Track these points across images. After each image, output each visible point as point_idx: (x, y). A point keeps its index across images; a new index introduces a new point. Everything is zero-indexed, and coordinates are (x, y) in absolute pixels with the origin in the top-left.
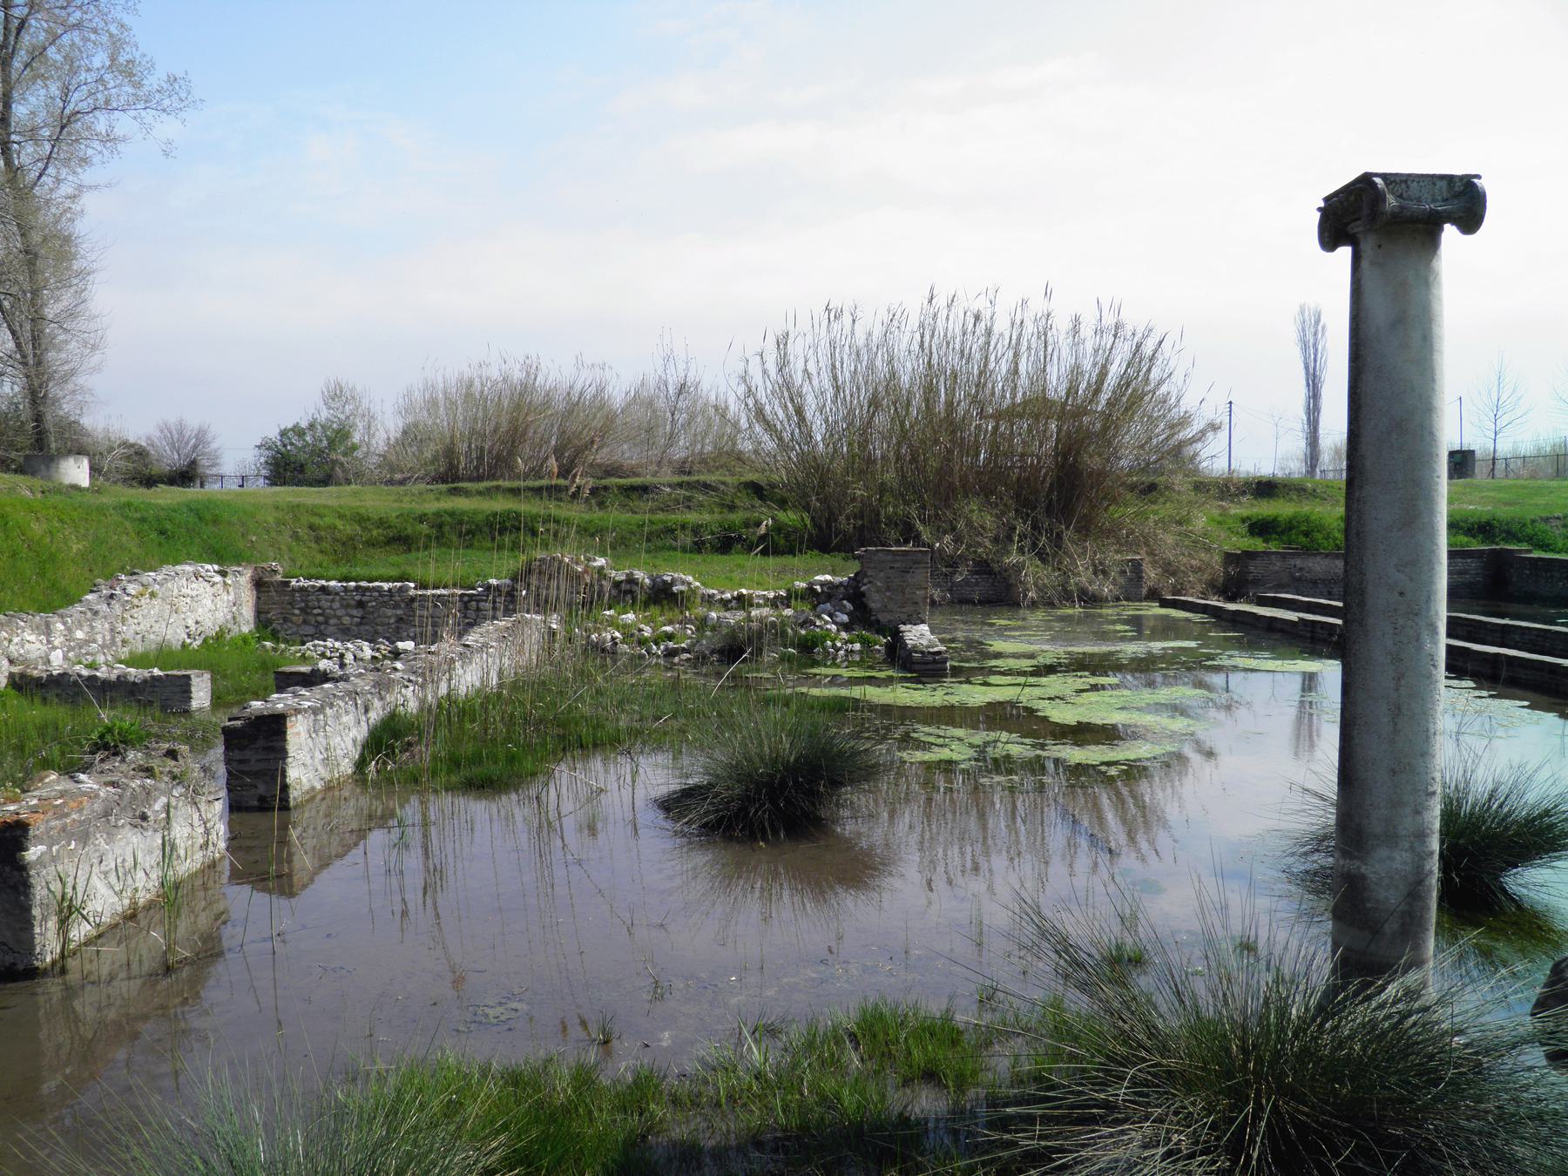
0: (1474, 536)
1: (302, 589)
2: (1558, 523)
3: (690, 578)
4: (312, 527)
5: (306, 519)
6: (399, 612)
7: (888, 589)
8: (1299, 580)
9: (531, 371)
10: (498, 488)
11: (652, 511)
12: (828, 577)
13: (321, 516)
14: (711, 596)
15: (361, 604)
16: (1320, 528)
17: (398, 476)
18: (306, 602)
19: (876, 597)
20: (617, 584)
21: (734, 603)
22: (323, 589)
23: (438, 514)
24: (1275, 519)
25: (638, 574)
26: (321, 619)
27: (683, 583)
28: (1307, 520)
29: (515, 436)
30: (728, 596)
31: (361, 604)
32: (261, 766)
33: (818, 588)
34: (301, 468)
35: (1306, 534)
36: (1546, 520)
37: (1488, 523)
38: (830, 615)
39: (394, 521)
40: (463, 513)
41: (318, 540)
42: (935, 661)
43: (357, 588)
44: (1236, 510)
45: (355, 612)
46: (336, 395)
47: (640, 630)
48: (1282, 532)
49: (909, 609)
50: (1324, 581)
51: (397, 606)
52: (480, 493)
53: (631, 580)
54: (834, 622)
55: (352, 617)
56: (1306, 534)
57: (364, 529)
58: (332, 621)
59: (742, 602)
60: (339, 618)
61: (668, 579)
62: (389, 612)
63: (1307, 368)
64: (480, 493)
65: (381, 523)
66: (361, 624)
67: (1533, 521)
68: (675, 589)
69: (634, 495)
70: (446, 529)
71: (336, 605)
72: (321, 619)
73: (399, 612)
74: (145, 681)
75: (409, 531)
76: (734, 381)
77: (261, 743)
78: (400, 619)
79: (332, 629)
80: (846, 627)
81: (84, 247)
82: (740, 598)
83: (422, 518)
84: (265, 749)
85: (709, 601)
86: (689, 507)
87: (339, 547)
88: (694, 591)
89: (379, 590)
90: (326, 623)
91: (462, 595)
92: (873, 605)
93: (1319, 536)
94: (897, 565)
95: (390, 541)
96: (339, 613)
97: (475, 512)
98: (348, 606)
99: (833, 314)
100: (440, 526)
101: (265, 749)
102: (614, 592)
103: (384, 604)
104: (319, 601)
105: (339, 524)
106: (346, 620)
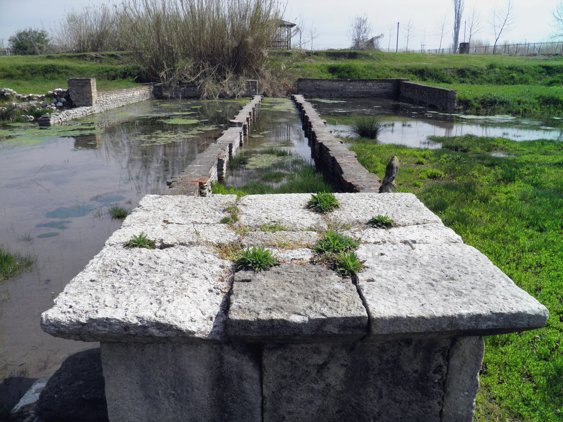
0: (416, 75)
2: (450, 70)
3: (11, 90)
7: (77, 93)
12: (60, 89)
14: (19, 97)
19: (73, 96)
27: (8, 92)
30: (26, 96)
33: (56, 93)
34: (26, 49)
35: (348, 72)
36: (446, 69)
37: (423, 70)
42: (45, 120)
44: (319, 63)
46: (360, 26)
48: (339, 72)
49: (86, 101)
50: (328, 90)
52: (58, 58)
54: (56, 106)
56: (348, 72)
59: (30, 98)
61: (3, 90)
63: (456, 10)
67: (441, 70)
68: (5, 94)
75: (13, 73)
85: (18, 98)
88: (13, 95)
92: (72, 99)
94: (80, 84)
95: (5, 77)
97: (39, 65)
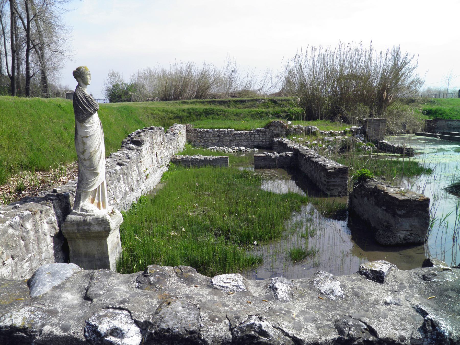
1: (200, 132)
3: (316, 127)
4: (152, 114)
5: (150, 111)
6: (230, 138)
8: (450, 128)
9: (189, 67)
10: (197, 101)
11: (244, 108)
13: (154, 111)
15: (219, 136)
16: (444, 113)
17: (150, 99)
18: (202, 135)
20: (295, 129)
21: (329, 135)
22: (207, 132)
23: (188, 109)
24: (431, 110)
25: (301, 126)
26: (206, 140)
27: (315, 129)
28: (441, 110)
29: (185, 86)
31: (219, 136)
32: (340, 183)
35: (441, 114)
38: (359, 138)
39: (175, 112)
40: (196, 109)
41: (154, 118)
43: (217, 131)
45: (217, 138)
46: (113, 75)
47: (307, 143)
51: (230, 136)
53: (299, 128)
55: (216, 140)
56: (441, 114)
57: (167, 114)
58: (210, 141)
59: (331, 134)
60: (212, 140)
62: (227, 138)
64: (191, 103)
65: (172, 112)
66: (219, 142)
69: (238, 103)
70: (192, 114)
71: (211, 136)
72: (206, 140)
73: (230, 138)
74: (213, 159)
76: (284, 69)
77: (340, 176)
78: (231, 140)
79: (209, 144)
80: (364, 141)
81: (60, 33)
82: (331, 133)
83: (183, 111)
84: (341, 178)
86: (255, 107)
87: (160, 120)
89: (224, 131)
90: (208, 142)
91: (250, 133)
93: (445, 115)
96: (212, 139)
98: (215, 136)
99: (314, 49)
100: (190, 113)
101: (341, 178)
102: (295, 132)
103: (226, 136)
104: (205, 135)
105: (159, 113)
106: (214, 141)
